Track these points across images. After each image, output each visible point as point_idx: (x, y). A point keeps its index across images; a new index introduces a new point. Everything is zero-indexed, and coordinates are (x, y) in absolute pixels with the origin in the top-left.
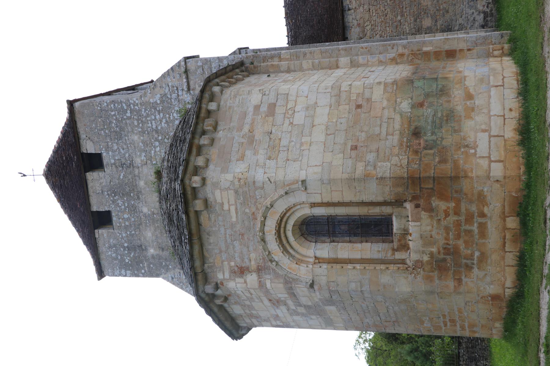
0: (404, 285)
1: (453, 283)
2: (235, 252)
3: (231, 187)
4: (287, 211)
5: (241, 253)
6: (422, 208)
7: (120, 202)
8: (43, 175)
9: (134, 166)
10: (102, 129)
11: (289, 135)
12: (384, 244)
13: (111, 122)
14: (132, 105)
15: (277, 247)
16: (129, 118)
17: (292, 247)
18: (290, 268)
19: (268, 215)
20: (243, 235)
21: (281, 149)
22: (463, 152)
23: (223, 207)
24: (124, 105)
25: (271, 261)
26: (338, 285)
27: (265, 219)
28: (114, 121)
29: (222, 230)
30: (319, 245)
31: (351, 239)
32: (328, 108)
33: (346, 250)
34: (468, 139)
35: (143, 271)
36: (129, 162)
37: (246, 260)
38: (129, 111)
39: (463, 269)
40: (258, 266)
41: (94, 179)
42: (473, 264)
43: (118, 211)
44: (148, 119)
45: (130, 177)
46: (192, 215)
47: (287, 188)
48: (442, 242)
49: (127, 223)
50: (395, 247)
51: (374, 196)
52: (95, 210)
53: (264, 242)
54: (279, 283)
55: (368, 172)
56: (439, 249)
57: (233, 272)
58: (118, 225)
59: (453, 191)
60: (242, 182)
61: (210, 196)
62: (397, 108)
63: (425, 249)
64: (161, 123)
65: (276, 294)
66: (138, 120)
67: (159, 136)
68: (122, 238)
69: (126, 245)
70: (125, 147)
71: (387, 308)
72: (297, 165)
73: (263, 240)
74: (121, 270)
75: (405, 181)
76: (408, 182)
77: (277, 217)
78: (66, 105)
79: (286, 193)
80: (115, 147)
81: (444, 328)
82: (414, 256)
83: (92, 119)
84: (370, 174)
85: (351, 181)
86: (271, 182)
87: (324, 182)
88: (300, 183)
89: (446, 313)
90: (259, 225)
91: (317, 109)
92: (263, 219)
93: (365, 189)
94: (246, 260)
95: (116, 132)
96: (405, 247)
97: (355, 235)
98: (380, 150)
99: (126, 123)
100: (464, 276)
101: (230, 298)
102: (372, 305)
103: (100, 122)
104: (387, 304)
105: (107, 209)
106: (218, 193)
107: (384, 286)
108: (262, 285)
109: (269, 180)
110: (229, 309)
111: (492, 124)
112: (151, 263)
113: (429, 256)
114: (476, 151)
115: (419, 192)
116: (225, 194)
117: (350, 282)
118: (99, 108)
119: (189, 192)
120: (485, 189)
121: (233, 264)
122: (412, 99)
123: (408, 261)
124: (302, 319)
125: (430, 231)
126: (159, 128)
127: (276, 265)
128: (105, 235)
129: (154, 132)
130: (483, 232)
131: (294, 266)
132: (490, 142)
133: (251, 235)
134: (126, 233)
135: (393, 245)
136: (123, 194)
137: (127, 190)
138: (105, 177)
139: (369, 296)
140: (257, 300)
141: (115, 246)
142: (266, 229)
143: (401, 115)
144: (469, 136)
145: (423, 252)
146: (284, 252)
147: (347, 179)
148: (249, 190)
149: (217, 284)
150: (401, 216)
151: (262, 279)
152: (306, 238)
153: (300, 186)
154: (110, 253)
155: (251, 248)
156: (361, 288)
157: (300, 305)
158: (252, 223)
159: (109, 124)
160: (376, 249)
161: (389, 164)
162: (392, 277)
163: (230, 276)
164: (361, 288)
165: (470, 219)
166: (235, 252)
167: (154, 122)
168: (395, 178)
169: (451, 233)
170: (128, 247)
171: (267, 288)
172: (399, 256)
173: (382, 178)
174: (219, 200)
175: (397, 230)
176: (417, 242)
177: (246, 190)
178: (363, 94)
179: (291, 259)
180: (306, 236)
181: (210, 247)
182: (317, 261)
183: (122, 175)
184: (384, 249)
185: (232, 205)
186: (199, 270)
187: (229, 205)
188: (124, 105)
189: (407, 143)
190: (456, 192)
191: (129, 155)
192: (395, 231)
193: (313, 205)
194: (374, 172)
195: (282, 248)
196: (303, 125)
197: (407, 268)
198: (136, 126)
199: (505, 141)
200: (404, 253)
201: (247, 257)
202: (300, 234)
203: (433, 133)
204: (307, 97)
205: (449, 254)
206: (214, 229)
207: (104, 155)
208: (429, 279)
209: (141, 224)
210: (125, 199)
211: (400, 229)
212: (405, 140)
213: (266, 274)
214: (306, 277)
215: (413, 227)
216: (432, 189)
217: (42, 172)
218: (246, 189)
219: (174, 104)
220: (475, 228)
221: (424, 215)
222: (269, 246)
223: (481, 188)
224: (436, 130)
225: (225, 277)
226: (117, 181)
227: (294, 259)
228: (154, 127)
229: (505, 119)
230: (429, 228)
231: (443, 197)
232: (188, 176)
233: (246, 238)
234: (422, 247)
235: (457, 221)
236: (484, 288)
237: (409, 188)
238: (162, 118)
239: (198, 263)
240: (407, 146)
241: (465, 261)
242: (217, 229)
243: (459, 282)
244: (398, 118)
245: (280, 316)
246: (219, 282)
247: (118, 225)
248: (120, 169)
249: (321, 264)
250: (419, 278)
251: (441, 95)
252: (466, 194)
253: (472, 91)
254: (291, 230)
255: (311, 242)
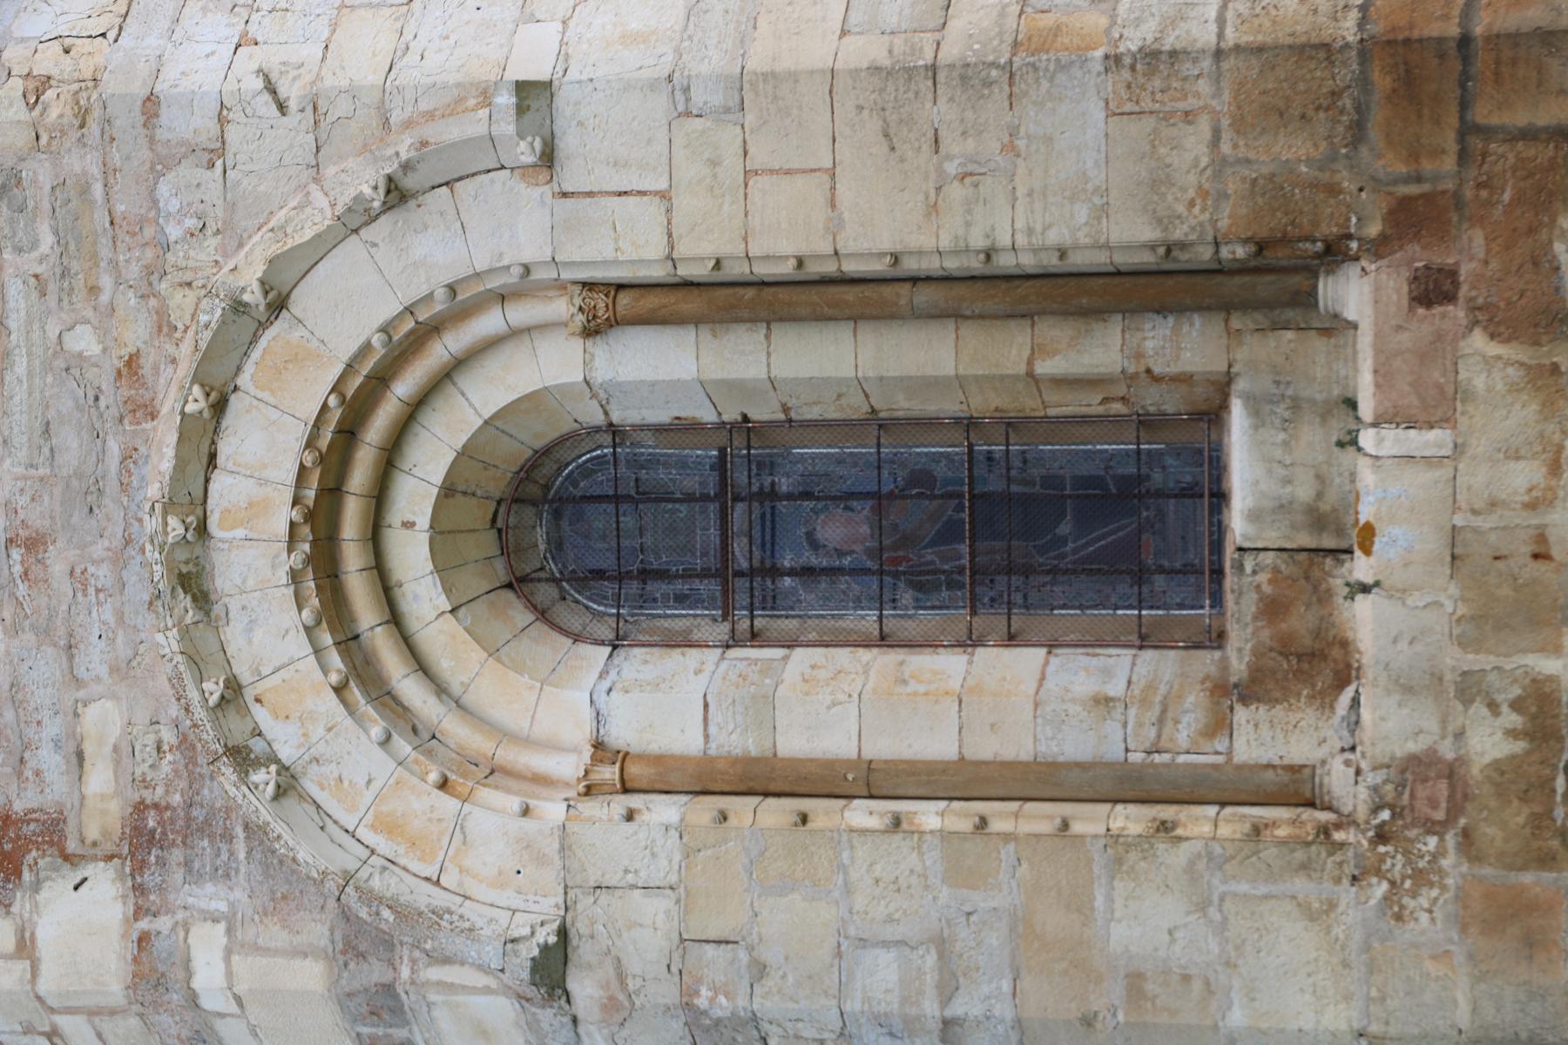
6: (1473, 308)
12: (1148, 655)
15: (299, 645)
17: (421, 666)
18: (390, 826)
19: (244, 380)
25: (242, 758)
26: (760, 970)
27: (219, 407)
30: (638, 663)
31: (890, 625)
33: (834, 693)
37: (49, 760)
40: (140, 807)
47: (404, 147)
51: (1082, 213)
53: (203, 600)
55: (1047, 21)
60: (57, 107)
63: (1484, 661)
73: (193, 583)
75: (1346, 72)
76: (1364, 81)
77: (312, 391)
82: (1391, 724)
84: (1057, 30)
86: (282, 108)
87: (698, 98)
88: (506, 99)
90: (163, 459)
92: (197, 404)
94: (49, 760)
96: (1314, 664)
97: (926, 585)
107: (1135, 983)
108: (154, 974)
109: (271, 89)
113: (1512, 719)
115: (1449, 164)
117: (863, 943)
123: (1338, 780)
125: (1532, 506)
127: (280, 793)
131: (425, 804)
133: (98, 550)
135: (1224, 661)
142: (225, 490)
145: (1469, 688)
146: (355, 693)
147: (875, 69)
148: (108, 172)
150: (1296, 405)
151: (163, 923)
152: (543, 614)
153: (506, 127)
155: (94, 659)
156: (945, 1001)
158: (114, 448)
162: (1202, 907)
164: (945, 1001)
168: (1260, 50)
171: (193, 999)
172: (1262, 738)
173: (1151, 57)
175: (1254, 516)
176: (1416, 600)
179: (403, 746)
180: (545, 593)
182: (609, 773)
184: (1151, 687)
192: (1238, 525)
193: (613, 305)
195: (335, 660)
197: (1324, 831)
200: (1307, 716)
201: (52, 728)
202: (500, 571)
211: (1283, 507)
213: (192, 874)
214: (508, 898)
215: (1393, 482)
218: (82, 163)
221: (1489, 362)
222: (234, 636)
227: (429, 753)
230: (1524, 476)
233: (58, 568)
234: (1463, 643)
237: (1374, 134)
249: (635, 801)
250: (1429, 918)
254: (423, 521)
255: (577, 638)
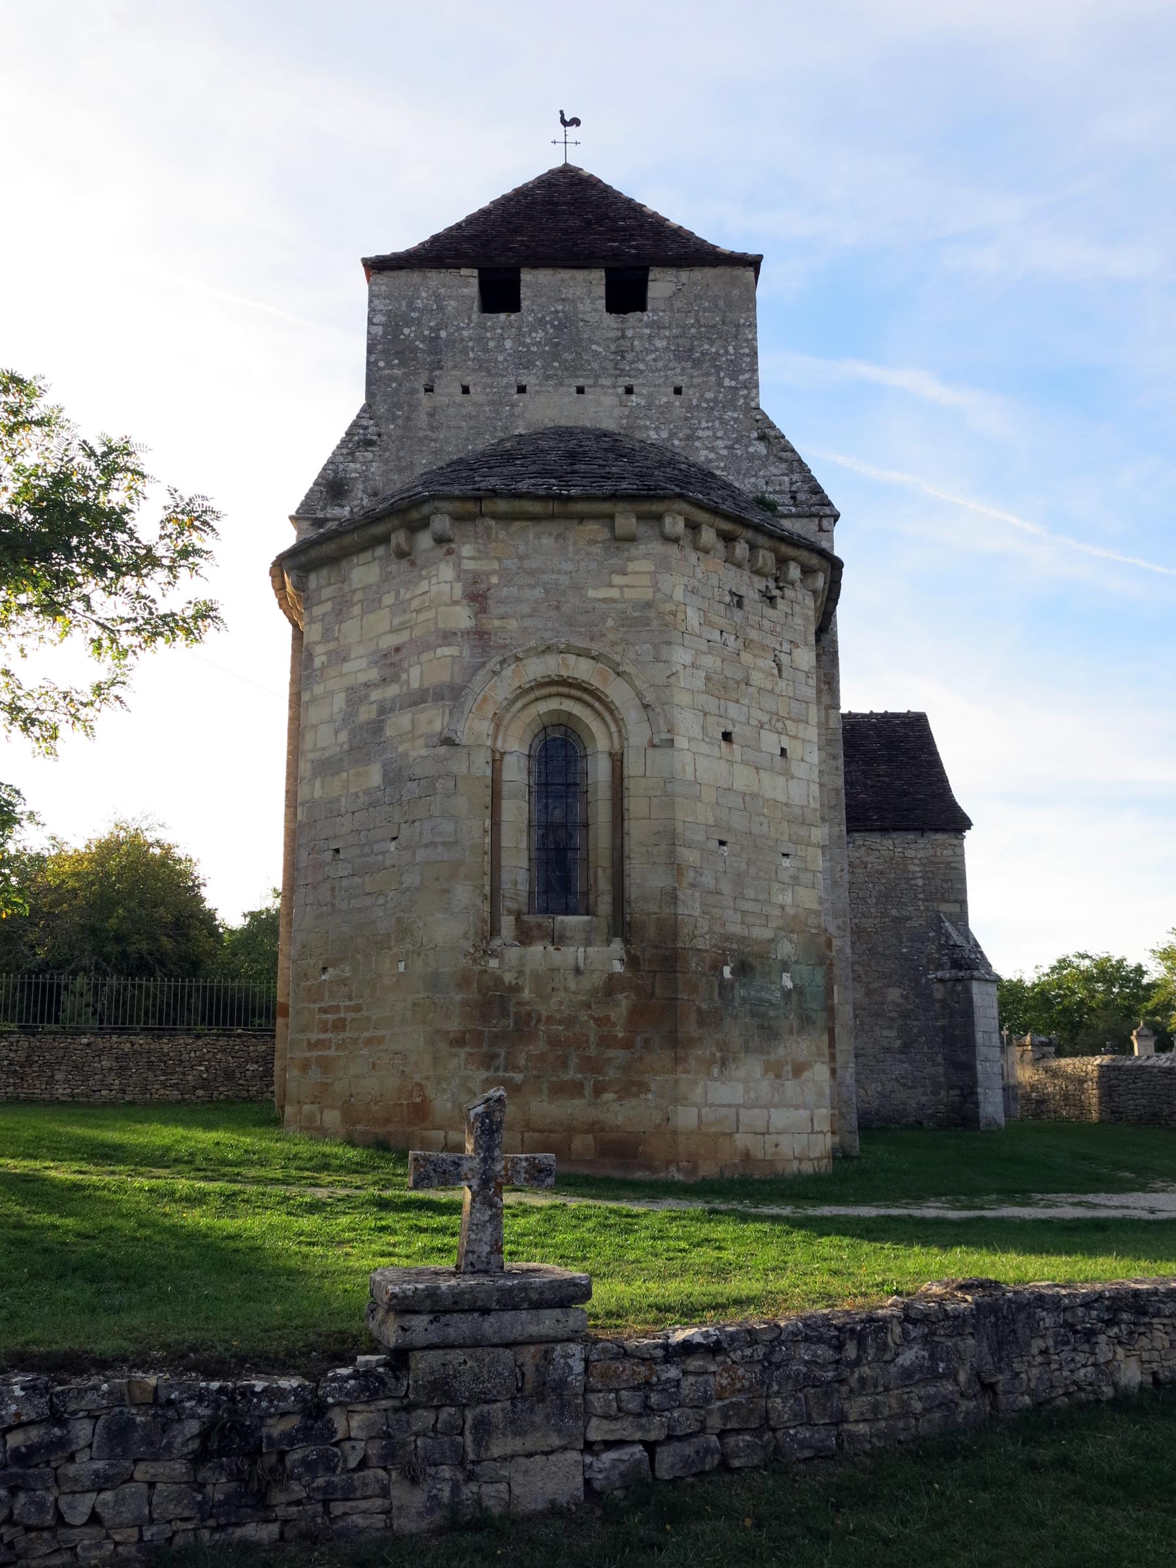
0: (448, 929)
1: (456, 1029)
2: (520, 587)
3: (659, 595)
4: (609, 707)
5: (518, 600)
7: (539, 335)
8: (566, 164)
9: (567, 368)
10: (698, 321)
11: (744, 720)
13: (712, 342)
14: (746, 392)
15: (532, 677)
16: (720, 384)
17: (525, 707)
18: (485, 700)
19: (600, 665)
20: (557, 608)
21: (722, 702)
22: (713, 1055)
23: (618, 573)
24: (747, 376)
27: (593, 658)
28: (714, 350)
29: (569, 567)
30: (524, 762)
32: (784, 801)
33: (516, 812)
34: (734, 1067)
35: (382, 364)
36: (628, 368)
37: (502, 610)
38: (733, 383)
39: (485, 1049)
41: (585, 289)
42: (497, 1069)
43: (519, 328)
44: (717, 423)
45: (595, 366)
46: (606, 507)
48: (543, 1010)
49: (492, 344)
50: (525, 918)
52: (523, 276)
53: (543, 652)
54: (452, 674)
56: (528, 1003)
57: (476, 578)
58: (489, 324)
59: (647, 1035)
61: (642, 549)
62: (783, 933)
64: (707, 448)
65: (419, 663)
66: (715, 400)
67: (681, 440)
68: (459, 329)
69: (443, 334)
70: (660, 364)
71: (381, 893)
72: (696, 732)
73: (548, 649)
74: (384, 315)
77: (596, 683)
78: (752, 251)
79: (646, 707)
80: (659, 344)
81: (316, 1006)
83: (721, 303)
85: (671, 838)
87: (669, 785)
88: (669, 736)
89: (364, 1013)
91: (782, 779)
92: (594, 653)
93: (654, 863)
94: (502, 610)
95: (691, 350)
96: (525, 937)
98: (719, 897)
99: (708, 374)
100: (471, 1051)
101: (404, 564)
102: (388, 863)
103: (713, 318)
104: (392, 894)
105: (525, 304)
106: (646, 566)
110: (366, 556)
111: (756, 1111)
112: (400, 385)
113: (514, 982)
114: (716, 1080)
116: (646, 580)
118: (742, 321)
119: (656, 507)
120: (650, 1096)
121: (494, 580)
122: (796, 962)
124: (336, 710)
126: (697, 444)
128: (465, 290)
129: (689, 432)
130: (560, 1090)
131: (490, 709)
132: (729, 1106)
134: (471, 339)
136: (558, 344)
137: (566, 356)
138: (596, 310)
139: (418, 859)
140: (396, 621)
141: (441, 308)
142: (571, 659)
143: (773, 940)
144: (738, 1068)
145: (521, 973)
149: (450, 541)
150: (590, 932)
154: (424, 295)
157: (382, 711)
159: (708, 338)
160: (519, 879)
161: (697, 914)
163: (467, 571)
165: (592, 1066)
166: (520, 587)
167: (710, 433)
168: (676, 923)
169: (561, 1028)
170: (438, 337)
172: (507, 923)
173: (675, 898)
174: (632, 566)
175: (562, 921)
177: (650, 621)
178: (806, 870)
180: (541, 736)
181: (531, 536)
182: (498, 757)
183: (600, 349)
185: (622, 593)
186: (487, 506)
187: (621, 587)
188: (747, 376)
189: (730, 950)
190: (647, 1041)
191: (642, 372)
193: (617, 761)
194: (685, 884)
195: (528, 686)
196: (759, 750)
198: (702, 396)
199: (730, 1135)
200: (512, 934)
203: (744, 1000)
204: (802, 760)
205: (516, 1022)
206: (571, 548)
207: (646, 317)
208: (464, 980)
209: (490, 375)
210: (547, 348)
212: (735, 946)
216: (653, 995)
217: (574, 162)
219: (746, 482)
220: (571, 1075)
222: (535, 660)
223: (653, 1086)
224: (748, 1007)
225: (465, 561)
226: (585, 336)
228: (700, 433)
229: (763, 1134)
231: (637, 1014)
232: (686, 507)
233: (551, 614)
235: (587, 1041)
236: (444, 1090)
238: (717, 453)
239: (502, 506)
240: (724, 950)
241: (503, 1054)
242: (570, 555)
243: (457, 1042)
244: (768, 934)
245: (346, 665)
246: (453, 546)
247: (489, 324)
248: (613, 348)
251: (800, 1017)
252: (641, 1059)
253: (806, 1074)
254: (562, 708)
